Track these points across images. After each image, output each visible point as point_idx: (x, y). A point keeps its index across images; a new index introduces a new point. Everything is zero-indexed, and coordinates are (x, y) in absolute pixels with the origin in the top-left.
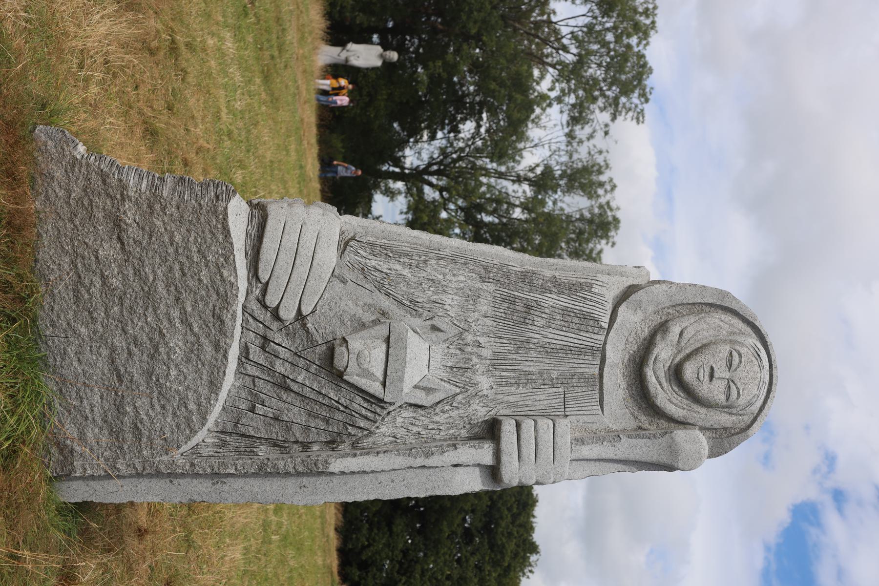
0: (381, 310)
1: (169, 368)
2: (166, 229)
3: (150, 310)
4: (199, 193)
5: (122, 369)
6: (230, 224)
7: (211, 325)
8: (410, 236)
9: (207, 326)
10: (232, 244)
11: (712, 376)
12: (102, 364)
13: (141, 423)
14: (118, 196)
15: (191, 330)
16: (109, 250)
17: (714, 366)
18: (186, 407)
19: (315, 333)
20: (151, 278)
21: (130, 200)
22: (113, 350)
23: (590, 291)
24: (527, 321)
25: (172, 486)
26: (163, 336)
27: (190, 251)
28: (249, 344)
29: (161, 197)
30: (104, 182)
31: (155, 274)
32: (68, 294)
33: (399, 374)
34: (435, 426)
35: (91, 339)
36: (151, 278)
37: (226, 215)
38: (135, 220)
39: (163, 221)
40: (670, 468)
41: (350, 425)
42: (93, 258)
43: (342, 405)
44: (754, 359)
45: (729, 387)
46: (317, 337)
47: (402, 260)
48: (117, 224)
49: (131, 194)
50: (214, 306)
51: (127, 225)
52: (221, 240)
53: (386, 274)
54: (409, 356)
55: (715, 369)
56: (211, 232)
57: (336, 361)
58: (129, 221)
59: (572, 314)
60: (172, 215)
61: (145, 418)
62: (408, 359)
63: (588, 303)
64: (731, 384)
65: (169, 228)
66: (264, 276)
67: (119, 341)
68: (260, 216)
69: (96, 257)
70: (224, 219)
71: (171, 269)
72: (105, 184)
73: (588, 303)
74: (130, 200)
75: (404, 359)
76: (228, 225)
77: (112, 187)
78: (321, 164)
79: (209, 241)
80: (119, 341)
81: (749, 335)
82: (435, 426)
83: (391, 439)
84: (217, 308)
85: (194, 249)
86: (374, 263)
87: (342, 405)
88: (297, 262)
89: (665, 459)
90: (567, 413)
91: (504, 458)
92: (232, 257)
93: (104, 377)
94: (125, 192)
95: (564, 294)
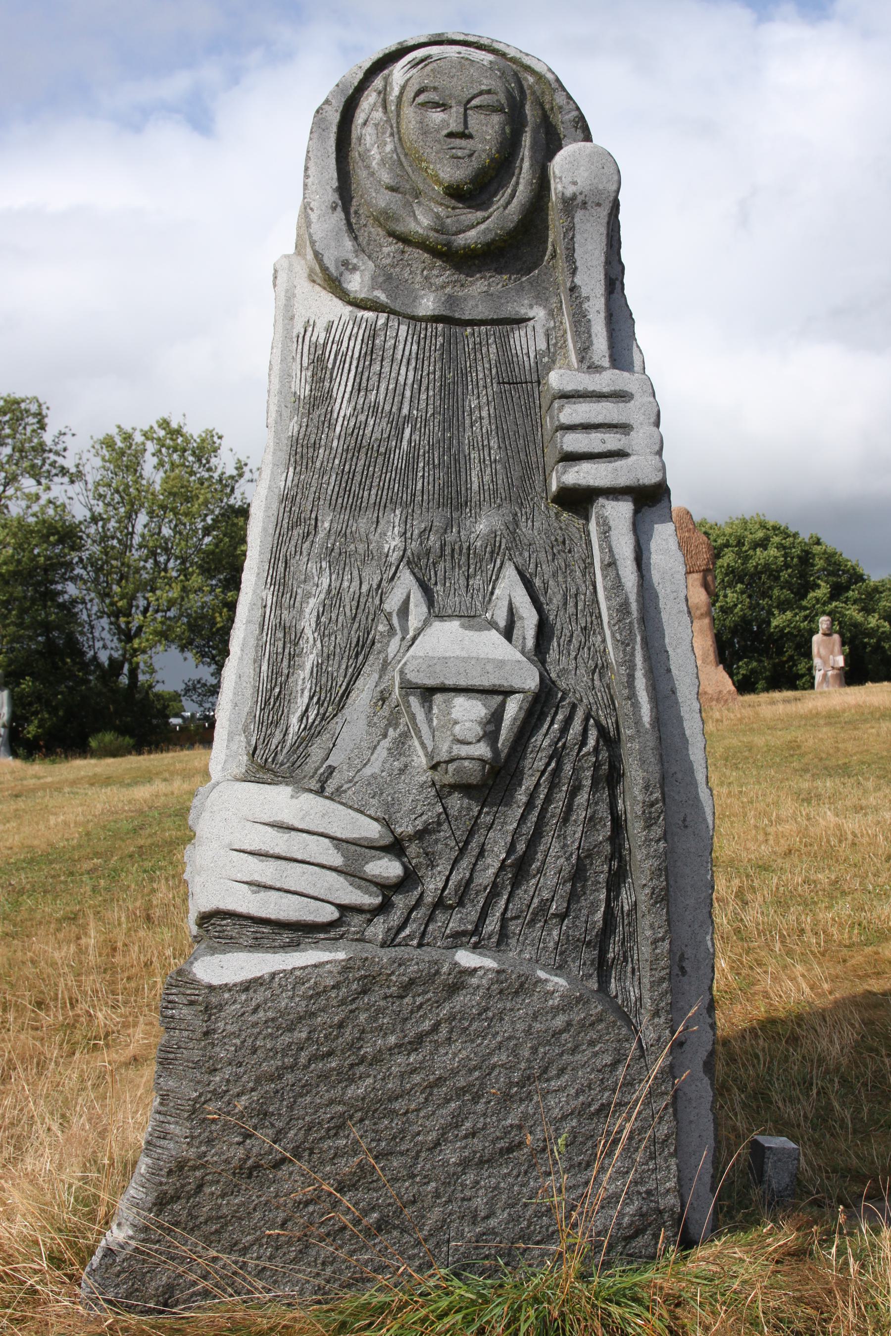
0: (376, 704)
1: (494, 1067)
2: (253, 1090)
3: (396, 1105)
4: (185, 1034)
5: (501, 1144)
6: (238, 979)
7: (419, 1000)
8: (241, 659)
9: (420, 1007)
10: (273, 975)
11: (464, 135)
12: (489, 1178)
13: (590, 1105)
14: (198, 1174)
15: (428, 1033)
16: (294, 1183)
17: (445, 132)
18: (561, 1032)
19: (424, 817)
20: (340, 1108)
21: (204, 1154)
22: (465, 1163)
23: (325, 345)
24: (382, 450)
25: (688, 1042)
26: (440, 1081)
27: (290, 1044)
28: (448, 931)
29: (195, 1100)
30: (176, 1198)
31: (331, 1102)
32: (374, 1245)
33: (489, 667)
34: (571, 603)
35: (449, 1201)
36: (340, 1108)
37: (226, 988)
38: (239, 1144)
39: (239, 1095)
40: (616, 206)
41: (580, 750)
42: (311, 1208)
43: (548, 764)
44: (429, 68)
45: (477, 107)
46: (429, 816)
47: (285, 671)
48: (250, 1171)
49: (192, 1153)
50: (386, 997)
51: (249, 1158)
52: (268, 993)
53: (311, 698)
54: (458, 653)
55: (449, 130)
56: (255, 1011)
57: (474, 780)
58: (241, 1152)
59: (366, 374)
60: (228, 1081)
61: (581, 1098)
62: (464, 654)
63: (344, 348)
64: (474, 102)
65: (251, 1085)
66: (329, 914)
67: (451, 1155)
68: (222, 927)
69: (307, 1203)
70: (230, 990)
71: (324, 1076)
72: (179, 1198)
73: (344, 348)
74: (204, 1154)
75: (465, 660)
76: (241, 983)
77: (183, 1186)
78: (520, 221)
79: (270, 1014)
80: (451, 1155)
81: (386, 79)
82: (571, 603)
83: (596, 676)
84: (389, 992)
85: (286, 1039)
86: (294, 720)
87: (548, 764)
88: (300, 857)
89: (604, 212)
90: (535, 378)
91: (623, 481)
92: (298, 973)
93: (515, 1173)
94: (191, 1163)
95: (330, 391)
